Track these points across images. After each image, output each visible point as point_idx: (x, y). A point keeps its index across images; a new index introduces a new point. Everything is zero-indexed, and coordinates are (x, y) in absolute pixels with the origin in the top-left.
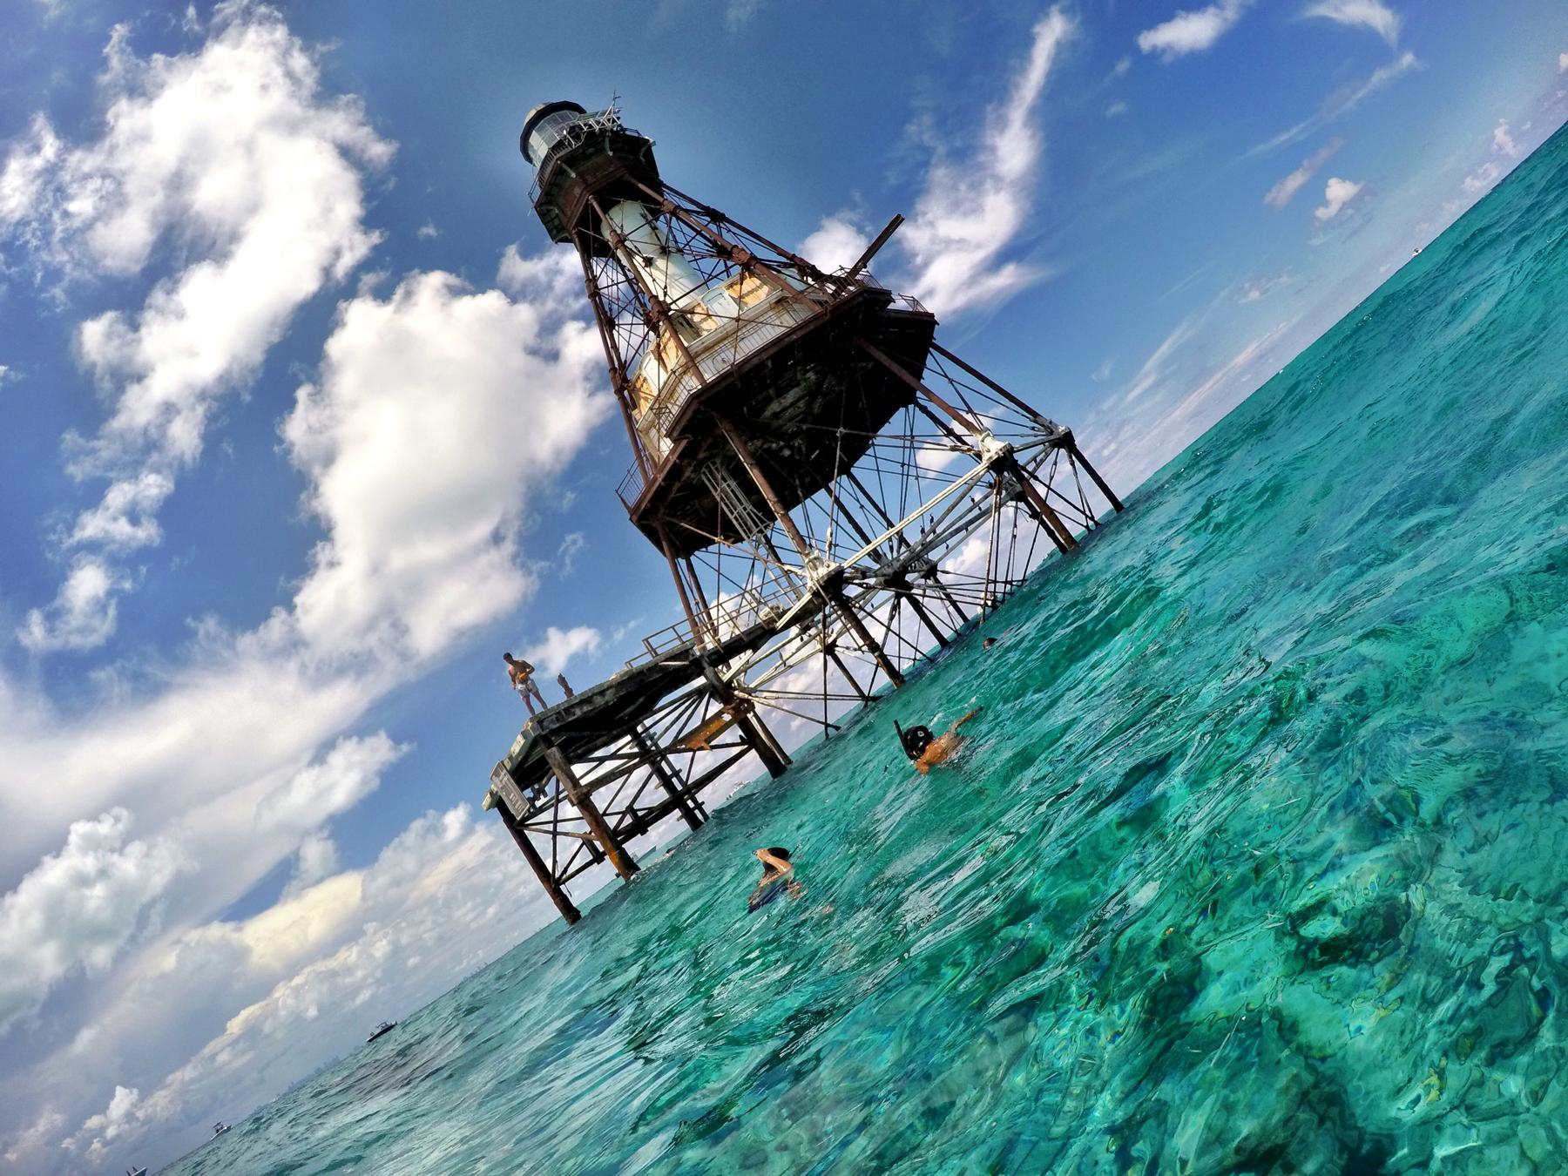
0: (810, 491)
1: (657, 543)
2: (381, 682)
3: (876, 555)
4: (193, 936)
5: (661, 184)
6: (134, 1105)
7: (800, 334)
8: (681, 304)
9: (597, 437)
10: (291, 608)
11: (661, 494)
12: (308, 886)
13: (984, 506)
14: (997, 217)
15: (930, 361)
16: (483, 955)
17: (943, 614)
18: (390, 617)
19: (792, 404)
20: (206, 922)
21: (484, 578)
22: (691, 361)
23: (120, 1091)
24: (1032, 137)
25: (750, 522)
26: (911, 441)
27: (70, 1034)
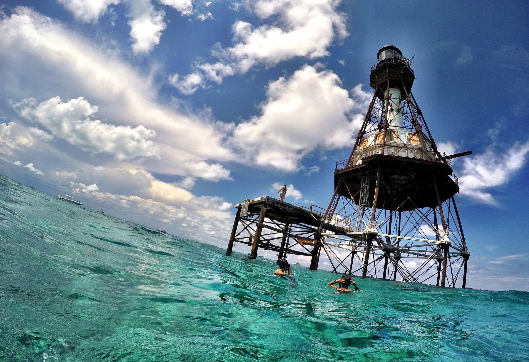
0: (386, 208)
1: (336, 185)
2: (244, 160)
3: (388, 239)
4: (143, 172)
5: (410, 91)
6: (95, 191)
7: (419, 162)
8: (393, 128)
9: (345, 148)
10: (237, 125)
12: (179, 187)
13: (428, 254)
14: (496, 177)
15: (448, 201)
16: (200, 239)
18: (258, 148)
19: (402, 180)
20: (149, 171)
21: (287, 159)
22: (384, 145)
23: (95, 185)
24: (524, 161)
25: (364, 201)
26: (424, 219)
27: (97, 165)
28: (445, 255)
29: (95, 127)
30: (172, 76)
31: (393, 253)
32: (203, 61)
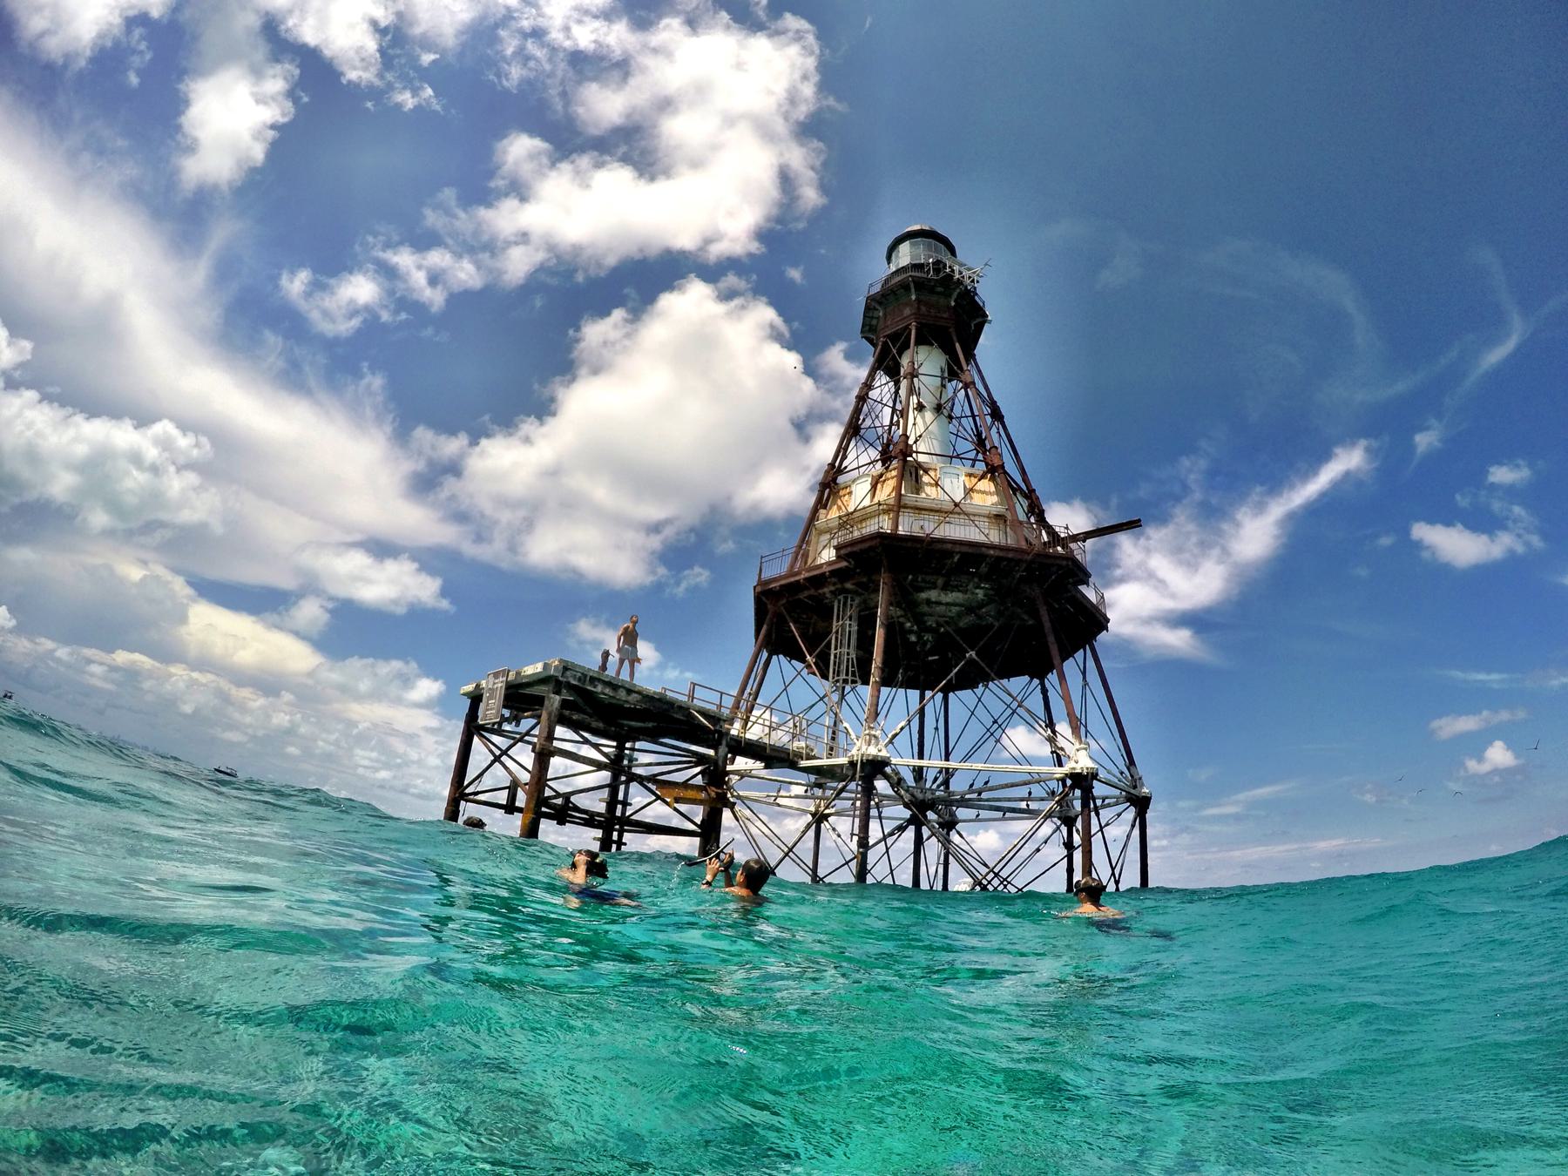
0: (908, 684)
2: (491, 552)
3: (919, 773)
7: (998, 553)
8: (922, 458)
9: (790, 518)
10: (474, 442)
11: (794, 588)
13: (1033, 806)
14: (1203, 584)
15: (1079, 655)
17: (932, 871)
18: (531, 511)
19: (947, 604)
21: (619, 547)
24: (1277, 537)
25: (843, 667)
26: (1016, 709)
28: (1085, 805)
29: (19, 415)
30: (293, 273)
31: (932, 809)
32: (396, 238)
